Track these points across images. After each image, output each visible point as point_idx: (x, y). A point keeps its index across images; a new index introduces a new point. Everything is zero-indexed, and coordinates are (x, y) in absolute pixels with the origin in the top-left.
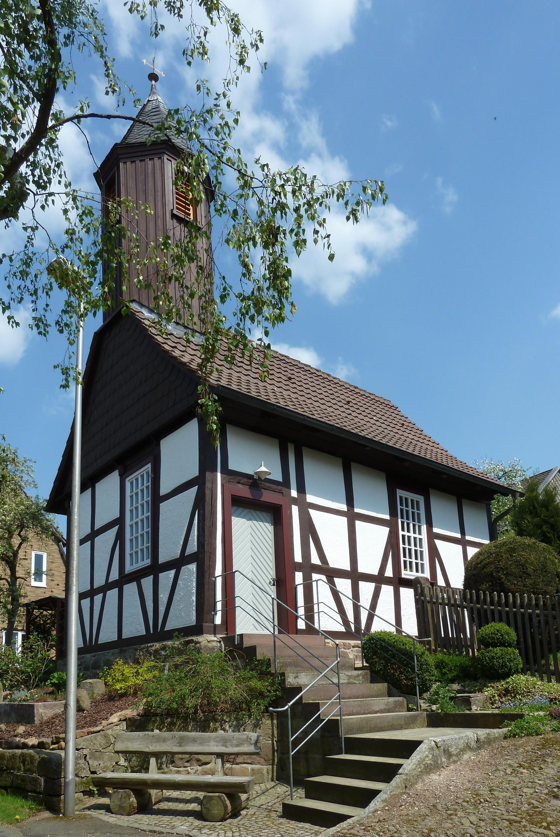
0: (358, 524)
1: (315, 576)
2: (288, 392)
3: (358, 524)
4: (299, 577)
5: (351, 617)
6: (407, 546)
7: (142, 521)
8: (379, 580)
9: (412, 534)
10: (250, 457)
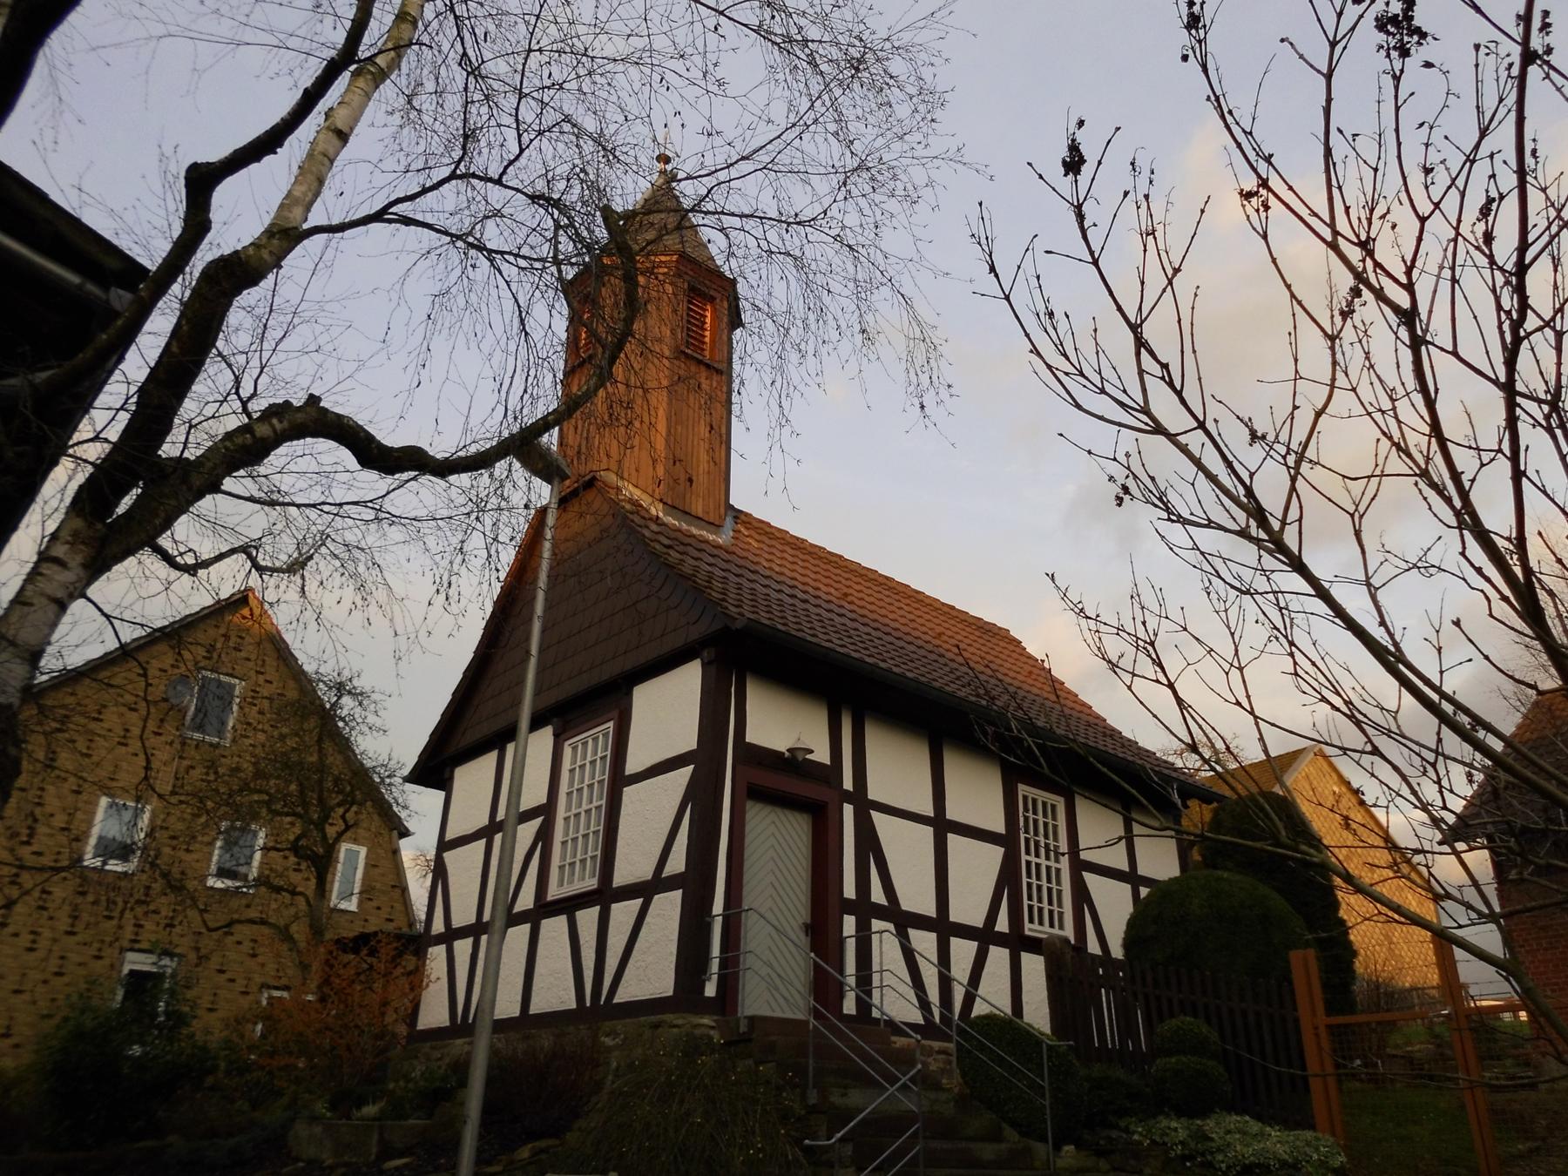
0: (952, 839)
1: (877, 924)
2: (843, 620)
3: (952, 839)
4: (849, 924)
5: (934, 995)
6: (1034, 880)
7: (588, 812)
8: (984, 936)
9: (1042, 861)
10: (779, 723)
